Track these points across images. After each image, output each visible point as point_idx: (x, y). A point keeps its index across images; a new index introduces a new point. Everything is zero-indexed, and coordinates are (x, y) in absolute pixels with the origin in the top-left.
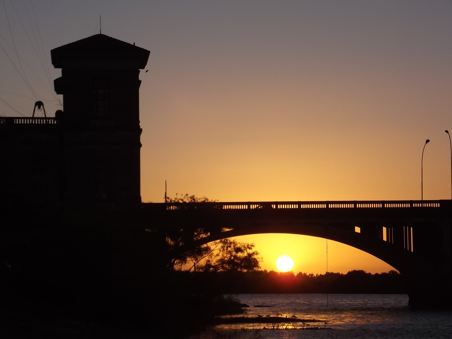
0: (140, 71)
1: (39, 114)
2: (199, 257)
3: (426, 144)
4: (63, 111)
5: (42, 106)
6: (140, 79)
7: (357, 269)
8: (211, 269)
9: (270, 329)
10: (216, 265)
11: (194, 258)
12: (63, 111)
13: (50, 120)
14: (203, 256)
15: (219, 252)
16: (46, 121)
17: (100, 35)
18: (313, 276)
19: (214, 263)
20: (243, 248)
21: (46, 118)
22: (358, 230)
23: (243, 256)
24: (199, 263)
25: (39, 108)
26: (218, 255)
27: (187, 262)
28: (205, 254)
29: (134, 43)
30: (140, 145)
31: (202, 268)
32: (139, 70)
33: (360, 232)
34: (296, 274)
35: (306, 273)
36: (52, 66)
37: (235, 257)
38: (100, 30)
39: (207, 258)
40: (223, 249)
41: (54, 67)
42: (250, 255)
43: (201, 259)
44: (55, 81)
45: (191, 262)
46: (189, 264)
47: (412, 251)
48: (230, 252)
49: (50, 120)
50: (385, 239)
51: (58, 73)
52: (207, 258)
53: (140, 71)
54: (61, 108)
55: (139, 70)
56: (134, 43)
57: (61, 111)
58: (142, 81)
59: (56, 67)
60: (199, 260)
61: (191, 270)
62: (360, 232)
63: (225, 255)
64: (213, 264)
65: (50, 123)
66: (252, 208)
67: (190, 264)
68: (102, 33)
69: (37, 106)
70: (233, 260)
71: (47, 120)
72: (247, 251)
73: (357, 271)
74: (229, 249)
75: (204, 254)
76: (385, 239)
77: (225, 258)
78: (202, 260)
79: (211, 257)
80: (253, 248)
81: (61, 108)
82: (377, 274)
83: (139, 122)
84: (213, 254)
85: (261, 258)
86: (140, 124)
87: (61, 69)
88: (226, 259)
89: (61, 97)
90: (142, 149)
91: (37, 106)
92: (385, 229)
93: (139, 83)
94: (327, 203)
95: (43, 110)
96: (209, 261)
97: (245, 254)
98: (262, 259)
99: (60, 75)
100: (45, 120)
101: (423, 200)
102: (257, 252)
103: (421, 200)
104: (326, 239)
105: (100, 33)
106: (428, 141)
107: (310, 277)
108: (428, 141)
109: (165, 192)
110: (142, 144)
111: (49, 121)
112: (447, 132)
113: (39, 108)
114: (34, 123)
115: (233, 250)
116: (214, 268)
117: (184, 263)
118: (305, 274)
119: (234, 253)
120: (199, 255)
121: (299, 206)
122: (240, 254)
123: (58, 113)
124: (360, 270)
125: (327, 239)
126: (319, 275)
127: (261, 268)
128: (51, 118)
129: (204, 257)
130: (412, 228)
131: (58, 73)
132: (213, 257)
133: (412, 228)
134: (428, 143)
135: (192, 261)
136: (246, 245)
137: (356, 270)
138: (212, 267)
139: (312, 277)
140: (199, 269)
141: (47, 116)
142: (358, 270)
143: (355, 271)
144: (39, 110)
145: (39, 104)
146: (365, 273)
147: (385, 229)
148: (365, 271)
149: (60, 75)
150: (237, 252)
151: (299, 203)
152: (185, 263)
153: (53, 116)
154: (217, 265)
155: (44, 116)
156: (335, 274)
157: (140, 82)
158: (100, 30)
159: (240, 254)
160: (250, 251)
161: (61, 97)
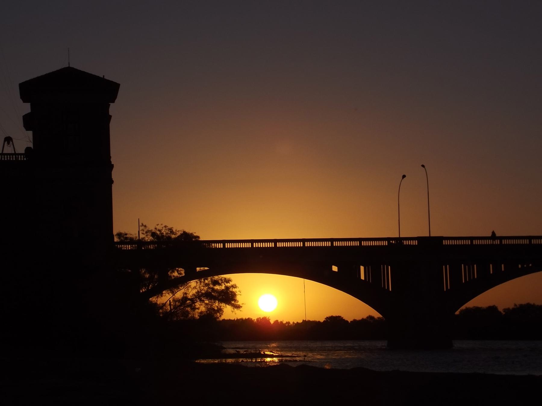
0: (110, 104)
1: (8, 150)
2: (175, 289)
3: (403, 180)
4: (32, 147)
5: (11, 142)
6: (110, 114)
7: (334, 315)
8: (188, 302)
9: (249, 362)
10: (192, 297)
11: (170, 290)
12: (32, 147)
13: (20, 156)
14: (179, 288)
15: (196, 284)
16: (16, 157)
17: (69, 67)
18: (290, 325)
19: (191, 296)
20: (220, 282)
21: (15, 154)
22: (335, 269)
23: (220, 289)
24: (175, 296)
25: (8, 143)
26: (195, 288)
27: (163, 295)
28: (181, 287)
29: (104, 76)
30: (112, 182)
31: (178, 300)
32: (109, 103)
33: (337, 271)
34: (272, 322)
35: (282, 321)
36: (21, 101)
37: (213, 289)
38: (69, 63)
39: (183, 291)
40: (200, 281)
41: (25, 130)
42: (227, 288)
43: (178, 292)
44: (23, 116)
45: (167, 294)
46: (166, 297)
47: (390, 290)
48: (207, 285)
49: (20, 156)
50: (363, 277)
51: (27, 108)
52: (183, 291)
53: (110, 104)
54: (31, 145)
55: (109, 103)
56: (104, 76)
57: (31, 147)
58: (112, 117)
59: (24, 102)
60: (175, 293)
61: (167, 303)
62: (337, 271)
63: (202, 288)
64: (189, 297)
65: (20, 159)
66: (260, 246)
67: (167, 297)
68: (70, 66)
69: (6, 142)
70: (210, 293)
71: (17, 156)
72: (225, 284)
73: (334, 316)
74: (206, 281)
75: (180, 286)
76: (363, 277)
77: (202, 290)
78: (178, 292)
79: (188, 289)
80: (230, 282)
81: (31, 145)
82: (355, 321)
83: (110, 157)
84: (191, 286)
85: (239, 291)
86: (112, 160)
87: (30, 103)
88: (203, 292)
89: (30, 133)
90: (114, 186)
91: (6, 142)
92: (362, 268)
93: (109, 118)
94: (304, 241)
95: (12, 146)
96: (186, 294)
97: (223, 287)
98: (240, 292)
99: (29, 111)
100: (14, 156)
101: (401, 237)
102: (236, 285)
103: (398, 237)
104: (303, 279)
105: (68, 66)
106: (404, 176)
107: (287, 325)
108: (404, 176)
109: (138, 230)
110: (114, 180)
111: (18, 157)
112: (423, 166)
113: (8, 143)
114: (3, 159)
115: (210, 282)
116: (191, 301)
117: (160, 296)
118: (281, 322)
119: (211, 286)
120: (175, 288)
121: (530, 242)
122: (217, 287)
123: (28, 149)
124: (337, 315)
125: (305, 279)
126: (295, 322)
127: (238, 302)
128: (21, 154)
129: (180, 290)
130: (389, 267)
131: (27, 108)
132: (190, 290)
133: (389, 267)
134: (404, 178)
135: (169, 294)
136: (223, 279)
137: (333, 315)
138: (189, 299)
139: (289, 325)
140: (176, 302)
141: (17, 152)
142: (335, 316)
143: (332, 316)
144: (8, 146)
145: (8, 140)
146: (343, 319)
147: (362, 268)
148: (342, 317)
149: (29, 111)
150: (214, 285)
151: (275, 241)
152: (162, 296)
153: (23, 152)
154: (193, 298)
155: (13, 152)
156: (311, 321)
157: (110, 117)
158: (69, 63)
159: (217, 287)
160: (228, 285)
161: (30, 133)
